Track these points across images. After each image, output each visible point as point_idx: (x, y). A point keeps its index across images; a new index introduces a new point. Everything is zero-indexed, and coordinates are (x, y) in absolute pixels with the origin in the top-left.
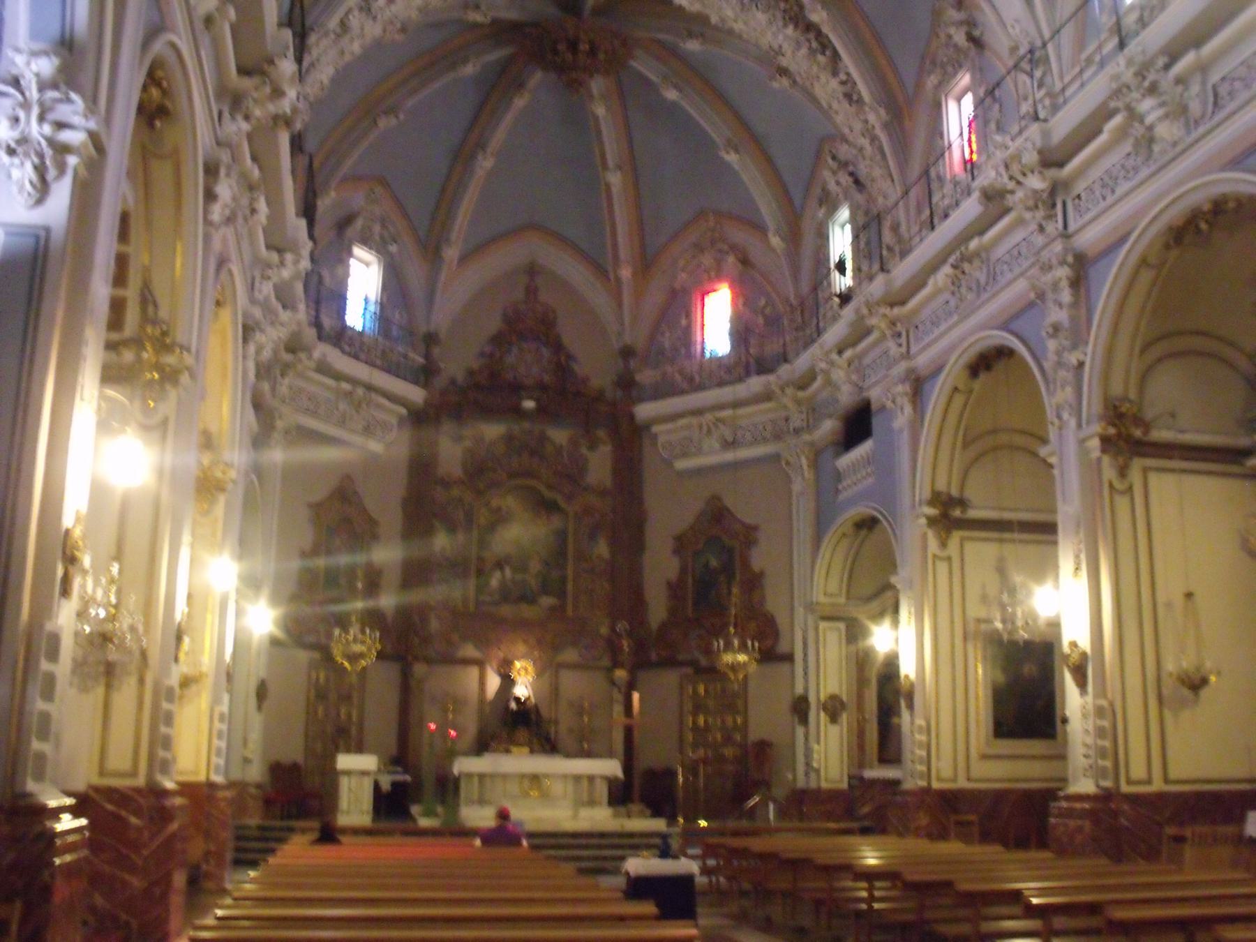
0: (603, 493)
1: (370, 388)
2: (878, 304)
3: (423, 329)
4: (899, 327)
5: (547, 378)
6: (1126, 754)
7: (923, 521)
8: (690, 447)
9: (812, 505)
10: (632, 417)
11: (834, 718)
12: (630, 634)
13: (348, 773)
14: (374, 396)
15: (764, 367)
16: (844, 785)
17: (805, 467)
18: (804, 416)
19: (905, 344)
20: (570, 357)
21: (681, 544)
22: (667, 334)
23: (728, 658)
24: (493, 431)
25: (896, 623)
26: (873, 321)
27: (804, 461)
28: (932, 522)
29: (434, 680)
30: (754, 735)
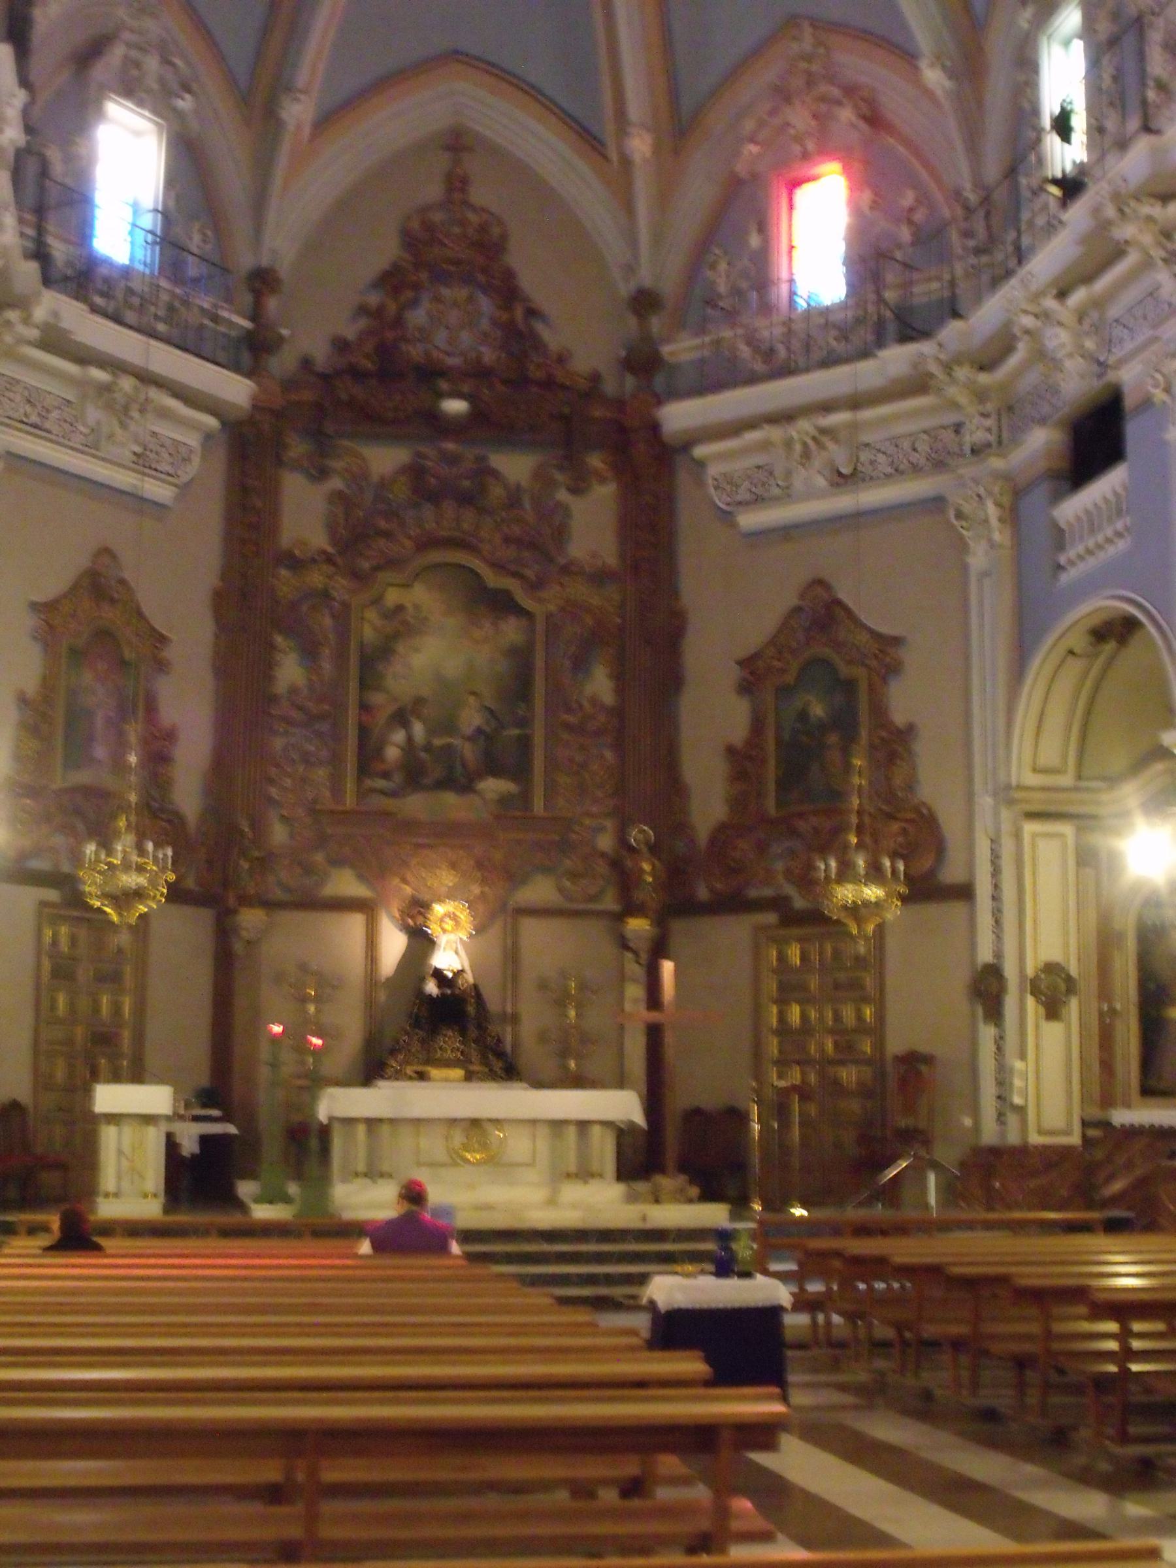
0: (600, 577)
1: (146, 378)
3: (245, 261)
5: (489, 356)
8: (769, 483)
10: (655, 428)
11: (1053, 1011)
12: (654, 849)
13: (114, 1119)
14: (153, 393)
15: (910, 327)
16: (1075, 1139)
22: (723, 266)
23: (846, 893)
24: (385, 459)
26: (1127, 231)
27: (992, 511)
29: (280, 941)
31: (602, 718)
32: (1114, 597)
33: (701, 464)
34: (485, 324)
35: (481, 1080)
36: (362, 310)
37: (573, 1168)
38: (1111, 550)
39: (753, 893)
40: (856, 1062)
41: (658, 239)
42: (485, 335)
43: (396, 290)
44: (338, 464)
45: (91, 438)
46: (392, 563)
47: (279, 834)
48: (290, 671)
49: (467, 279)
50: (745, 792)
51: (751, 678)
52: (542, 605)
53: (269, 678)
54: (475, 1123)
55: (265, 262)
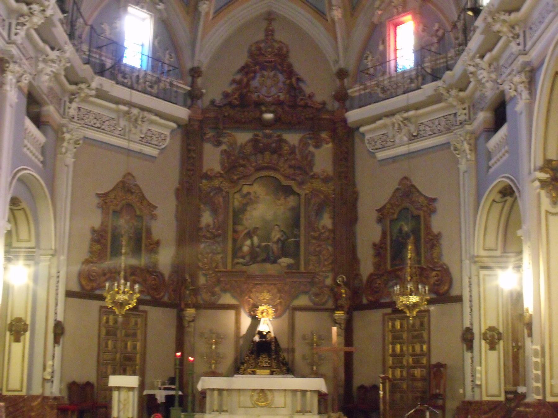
0: (326, 180)
1: (143, 109)
2: (498, 11)
3: (189, 65)
4: (517, 30)
5: (282, 96)
6: (8, 378)
7: (537, 184)
8: (389, 141)
9: (474, 183)
10: (345, 121)
11: (492, 347)
12: (346, 284)
13: (119, 388)
14: (146, 114)
15: (435, 76)
16: (502, 398)
17: (468, 151)
18: (466, 111)
19: (522, 43)
20: (299, 80)
21: (382, 215)
22: (370, 58)
23: (403, 300)
24: (243, 137)
25: (518, 267)
26: (497, 27)
27: (466, 146)
28: (544, 184)
29: (203, 322)
30: (434, 361)
31: (327, 234)
32: (503, 177)
33: (363, 135)
34: (281, 85)
35: (277, 374)
36: (234, 81)
37: (299, 409)
38: (504, 158)
39: (383, 301)
40: (421, 367)
41: (346, 49)
42: (281, 89)
43: (247, 73)
44: (225, 140)
45: (122, 131)
46: (245, 177)
47: (202, 280)
48: (207, 218)
49: (274, 68)
50: (378, 261)
51: (381, 216)
52: (303, 191)
53: (199, 221)
54: (262, 391)
55: (196, 65)
